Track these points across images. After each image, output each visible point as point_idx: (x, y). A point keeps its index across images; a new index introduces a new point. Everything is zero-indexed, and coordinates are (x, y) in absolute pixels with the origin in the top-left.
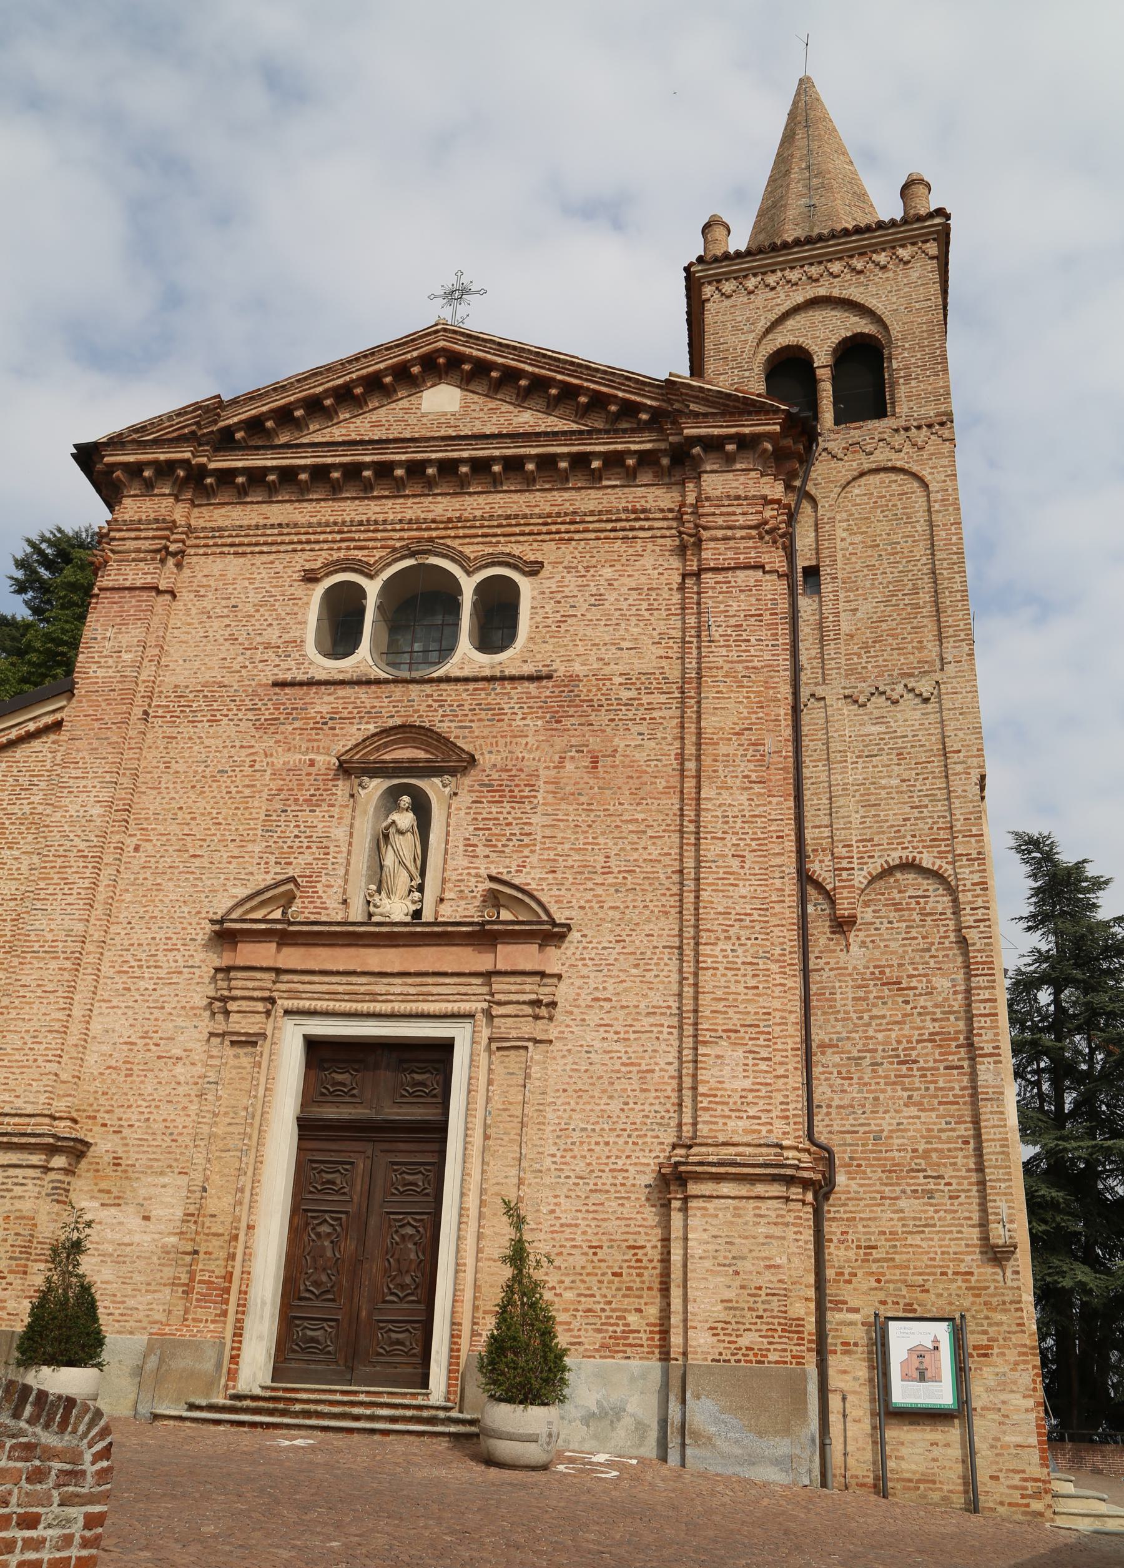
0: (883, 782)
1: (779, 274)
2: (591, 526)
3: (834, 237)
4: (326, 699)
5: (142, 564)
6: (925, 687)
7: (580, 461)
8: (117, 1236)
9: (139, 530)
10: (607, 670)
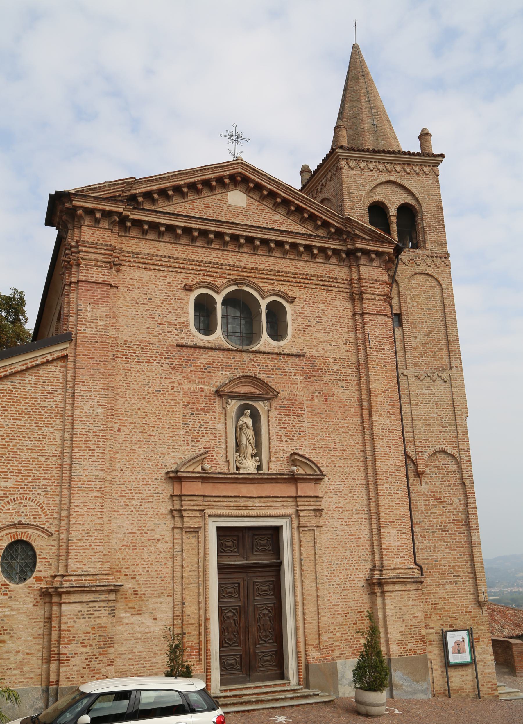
0: (431, 415)
1: (374, 164)
2: (314, 282)
3: (399, 154)
4: (204, 356)
5: (100, 269)
6: (445, 376)
7: (308, 248)
8: (142, 629)
9: (96, 248)
10: (327, 355)
